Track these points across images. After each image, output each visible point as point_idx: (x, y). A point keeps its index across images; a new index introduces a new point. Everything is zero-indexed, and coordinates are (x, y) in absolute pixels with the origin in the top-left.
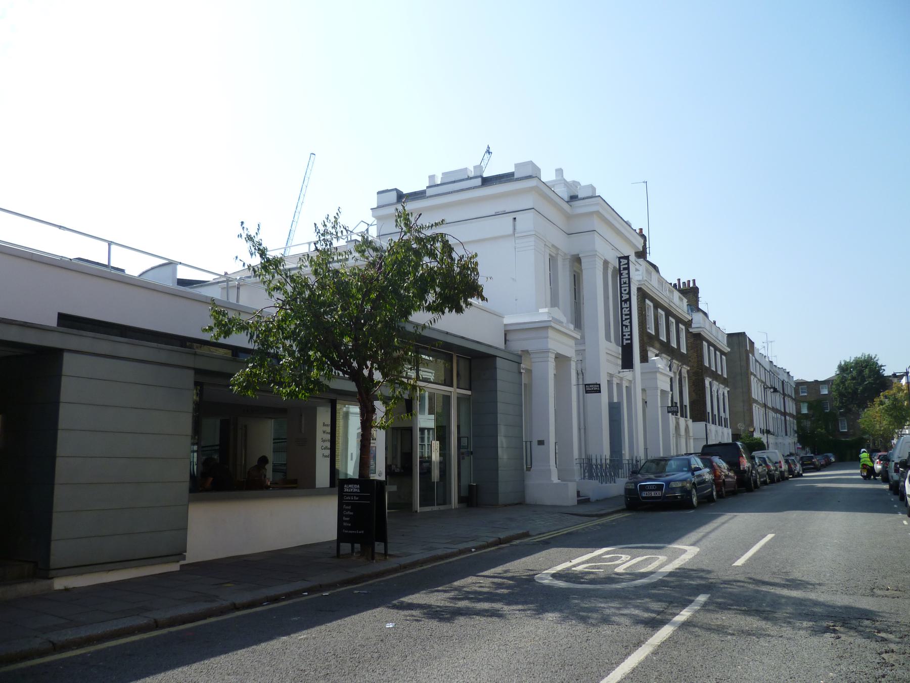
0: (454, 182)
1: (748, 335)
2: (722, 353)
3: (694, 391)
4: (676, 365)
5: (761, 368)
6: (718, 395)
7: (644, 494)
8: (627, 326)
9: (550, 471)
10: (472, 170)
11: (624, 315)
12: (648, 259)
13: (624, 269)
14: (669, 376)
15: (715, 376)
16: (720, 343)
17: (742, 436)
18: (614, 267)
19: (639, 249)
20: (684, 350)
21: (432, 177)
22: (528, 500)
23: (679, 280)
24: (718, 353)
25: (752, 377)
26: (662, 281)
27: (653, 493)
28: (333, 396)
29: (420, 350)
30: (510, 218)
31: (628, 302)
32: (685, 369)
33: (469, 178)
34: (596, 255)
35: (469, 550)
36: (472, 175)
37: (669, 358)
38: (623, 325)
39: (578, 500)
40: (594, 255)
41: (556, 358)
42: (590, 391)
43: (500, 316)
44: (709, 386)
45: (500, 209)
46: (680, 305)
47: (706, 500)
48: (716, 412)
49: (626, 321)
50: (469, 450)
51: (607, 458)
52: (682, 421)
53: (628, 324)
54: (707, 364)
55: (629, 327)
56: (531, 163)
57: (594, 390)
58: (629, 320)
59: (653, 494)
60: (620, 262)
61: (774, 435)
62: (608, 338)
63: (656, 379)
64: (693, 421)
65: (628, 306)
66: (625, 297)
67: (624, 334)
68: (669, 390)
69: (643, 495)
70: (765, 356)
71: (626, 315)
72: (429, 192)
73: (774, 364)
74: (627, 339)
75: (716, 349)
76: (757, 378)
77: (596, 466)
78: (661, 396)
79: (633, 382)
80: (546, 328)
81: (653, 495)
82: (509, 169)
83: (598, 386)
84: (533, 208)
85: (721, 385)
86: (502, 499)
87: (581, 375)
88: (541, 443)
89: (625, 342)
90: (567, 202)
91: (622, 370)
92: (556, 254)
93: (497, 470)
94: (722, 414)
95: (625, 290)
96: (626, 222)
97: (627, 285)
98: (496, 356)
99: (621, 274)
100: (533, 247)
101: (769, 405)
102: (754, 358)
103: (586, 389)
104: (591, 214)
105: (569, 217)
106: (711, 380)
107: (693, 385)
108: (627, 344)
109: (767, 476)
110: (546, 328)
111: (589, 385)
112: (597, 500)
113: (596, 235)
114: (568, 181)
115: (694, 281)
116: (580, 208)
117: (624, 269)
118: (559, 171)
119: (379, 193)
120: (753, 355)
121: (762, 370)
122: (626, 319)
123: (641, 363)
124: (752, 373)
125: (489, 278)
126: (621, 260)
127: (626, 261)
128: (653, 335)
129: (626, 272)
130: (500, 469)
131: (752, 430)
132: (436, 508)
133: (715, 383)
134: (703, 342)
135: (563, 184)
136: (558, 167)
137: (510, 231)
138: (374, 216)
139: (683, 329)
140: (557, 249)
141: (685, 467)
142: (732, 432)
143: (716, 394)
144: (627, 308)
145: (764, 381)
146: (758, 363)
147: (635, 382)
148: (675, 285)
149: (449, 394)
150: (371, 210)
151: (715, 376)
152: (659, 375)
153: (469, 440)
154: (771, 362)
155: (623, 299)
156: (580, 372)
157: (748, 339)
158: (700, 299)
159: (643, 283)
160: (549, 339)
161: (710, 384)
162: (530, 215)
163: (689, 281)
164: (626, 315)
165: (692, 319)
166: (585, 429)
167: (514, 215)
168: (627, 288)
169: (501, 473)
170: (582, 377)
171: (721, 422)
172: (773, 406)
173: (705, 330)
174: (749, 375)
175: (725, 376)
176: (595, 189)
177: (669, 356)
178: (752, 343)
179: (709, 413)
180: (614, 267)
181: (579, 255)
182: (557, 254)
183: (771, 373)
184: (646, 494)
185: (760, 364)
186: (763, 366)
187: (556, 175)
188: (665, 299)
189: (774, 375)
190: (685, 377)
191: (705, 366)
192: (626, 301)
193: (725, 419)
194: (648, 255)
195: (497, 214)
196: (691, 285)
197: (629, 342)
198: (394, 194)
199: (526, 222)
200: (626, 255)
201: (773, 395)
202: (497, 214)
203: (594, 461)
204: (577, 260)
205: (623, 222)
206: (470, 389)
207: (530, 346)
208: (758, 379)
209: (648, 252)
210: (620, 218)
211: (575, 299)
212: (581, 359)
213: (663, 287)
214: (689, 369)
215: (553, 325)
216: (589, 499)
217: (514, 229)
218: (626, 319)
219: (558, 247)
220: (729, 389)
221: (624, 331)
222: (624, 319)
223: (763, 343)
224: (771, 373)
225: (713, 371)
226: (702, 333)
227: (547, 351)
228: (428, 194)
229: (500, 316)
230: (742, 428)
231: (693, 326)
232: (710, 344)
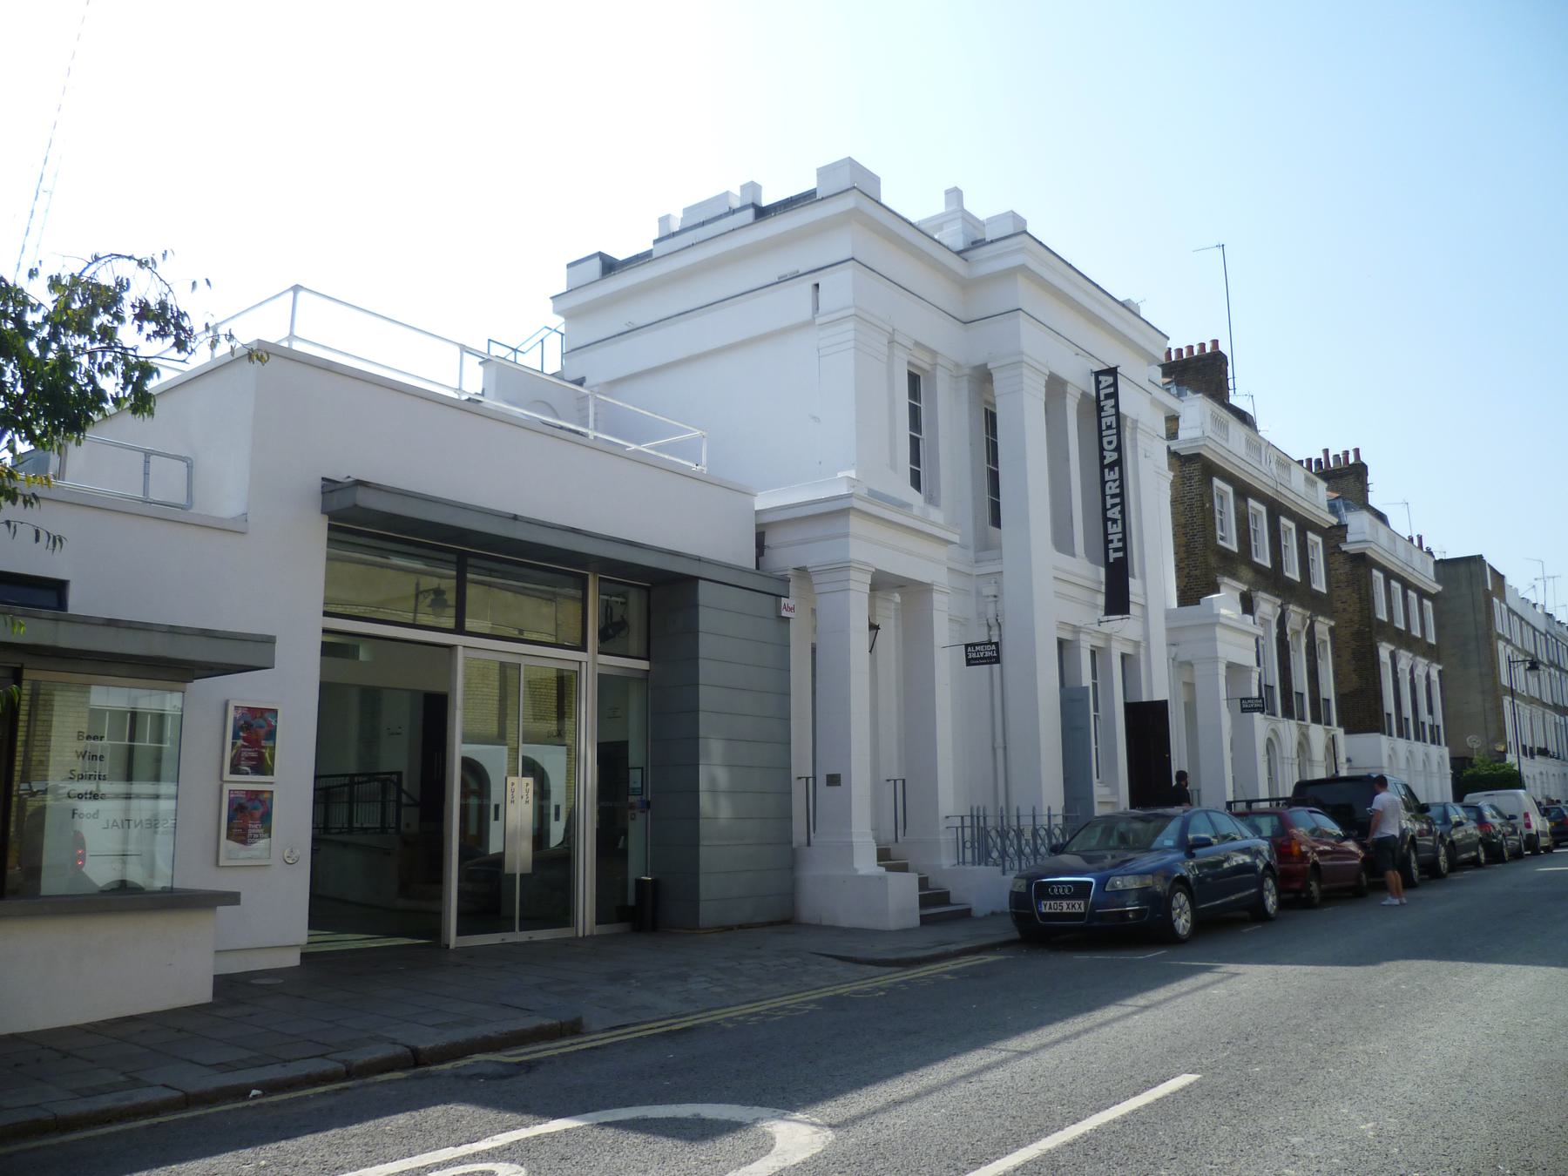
0: (703, 224)
1: (1488, 561)
2: (1422, 594)
3: (1355, 670)
4: (1300, 618)
5: (1525, 627)
6: (1412, 679)
7: (1047, 907)
8: (1115, 521)
9: (852, 846)
10: (738, 193)
11: (1108, 498)
12: (1233, 400)
13: (1108, 396)
14: (1253, 634)
15: (1404, 640)
16: (1415, 574)
17: (1474, 761)
18: (1084, 395)
19: (1159, 360)
20: (1320, 585)
21: (664, 221)
22: (807, 913)
23: (1326, 451)
24: (1395, 585)
25: (1501, 645)
26: (1258, 445)
27: (1065, 904)
28: (14, 660)
29: (471, 561)
30: (806, 285)
31: (1117, 469)
32: (1323, 626)
33: (733, 212)
34: (1022, 362)
35: (241, 1093)
36: (736, 204)
37: (1279, 602)
38: (1106, 519)
39: (921, 916)
41: (874, 588)
42: (976, 659)
43: (745, 493)
44: (1389, 662)
45: (788, 269)
46: (1316, 500)
47: (1246, 914)
48: (1407, 711)
49: (1113, 510)
50: (644, 798)
51: (987, 813)
52: (1317, 734)
53: (1118, 516)
54: (1382, 615)
55: (1119, 522)
56: (851, 163)
57: (986, 658)
58: (1119, 508)
59: (1065, 906)
60: (1098, 383)
61: (1558, 758)
62: (1062, 542)
63: (1214, 639)
64: (1347, 732)
65: (1117, 476)
66: (1111, 457)
67: (1110, 537)
68: (1255, 664)
69: (1044, 911)
70: (1535, 605)
71: (1113, 496)
73: (1557, 619)
74: (1116, 550)
75: (1406, 585)
76: (1513, 645)
78: (1227, 678)
79: (1143, 644)
80: (844, 513)
82: (807, 183)
83: (994, 647)
84: (853, 259)
85: (1419, 659)
86: (708, 912)
87: (997, 628)
88: (833, 780)
89: (1113, 556)
91: (1106, 618)
92: (931, 365)
93: (696, 845)
94: (1424, 716)
95: (1110, 443)
96: (1123, 304)
97: (1115, 431)
98: (697, 578)
99: (1100, 409)
100: (852, 344)
101: (1545, 701)
102: (1504, 606)
103: (967, 656)
104: (1011, 273)
105: (966, 286)
106: (1392, 648)
108: (1115, 559)
109: (1481, 848)
110: (844, 513)
111: (974, 645)
112: (993, 914)
113: (1024, 323)
114: (981, 219)
115: (1357, 451)
116: (987, 263)
117: (1108, 396)
118: (955, 195)
119: (569, 266)
120: (1503, 599)
121: (1528, 633)
122: (1113, 506)
124: (1500, 637)
125: (201, 284)
126: (1101, 378)
127: (1110, 380)
128: (1233, 552)
129: (1111, 402)
130: (703, 842)
131: (1502, 748)
132: (519, 936)
133: (1405, 659)
134: (1371, 571)
135: (960, 220)
136: (950, 186)
137: (805, 312)
138: (558, 312)
139: (1317, 544)
140: (933, 353)
141: (1439, 819)
142: (1450, 753)
143: (1408, 677)
144: (1114, 481)
145: (1533, 652)
146: (1515, 618)
147: (1148, 643)
148: (1319, 462)
149: (575, 667)
150: (551, 301)
151: (1404, 640)
152: (1219, 632)
153: (645, 773)
154: (1550, 616)
155: (1106, 462)
156: (992, 621)
157: (1488, 570)
158: (1371, 488)
159: (1202, 443)
160: (851, 539)
161: (1394, 657)
162: (846, 274)
163: (1346, 453)
164: (1113, 496)
166: (1005, 748)
167: (814, 279)
168: (1114, 438)
169: (709, 856)
170: (997, 632)
172: (1556, 701)
173: (1374, 547)
174: (1494, 639)
175: (1432, 640)
176: (962, 192)
177: (1278, 596)
178: (1499, 578)
179: (1389, 715)
180: (1084, 395)
181: (986, 365)
182: (934, 365)
183: (1548, 636)
184: (1050, 908)
185: (1521, 619)
186: (1528, 623)
187: (947, 203)
188: (1264, 479)
189: (1557, 640)
190: (1325, 642)
191: (1396, 628)
192: (1111, 466)
193: (1432, 727)
194: (1231, 392)
195: (783, 280)
196: (1352, 460)
197: (1120, 554)
198: (597, 262)
199: (839, 288)
200: (1112, 366)
201: (1530, 678)
202: (783, 280)
203: (991, 822)
204: (983, 377)
205: (1115, 304)
206: (647, 659)
207: (812, 557)
208: (1518, 649)
209: (1231, 386)
210: (1094, 288)
212: (993, 593)
213: (1261, 457)
214: (1332, 623)
215: (857, 504)
216: (969, 910)
217: (816, 308)
218: (1113, 506)
219: (935, 349)
220: (1440, 667)
221: (1110, 531)
222: (1108, 506)
223: (1536, 579)
224: (1548, 636)
225: (1399, 630)
226: (1369, 553)
227: (844, 567)
228: (655, 255)
229: (745, 493)
230: (1476, 746)
231: (1350, 538)
232: (1389, 575)
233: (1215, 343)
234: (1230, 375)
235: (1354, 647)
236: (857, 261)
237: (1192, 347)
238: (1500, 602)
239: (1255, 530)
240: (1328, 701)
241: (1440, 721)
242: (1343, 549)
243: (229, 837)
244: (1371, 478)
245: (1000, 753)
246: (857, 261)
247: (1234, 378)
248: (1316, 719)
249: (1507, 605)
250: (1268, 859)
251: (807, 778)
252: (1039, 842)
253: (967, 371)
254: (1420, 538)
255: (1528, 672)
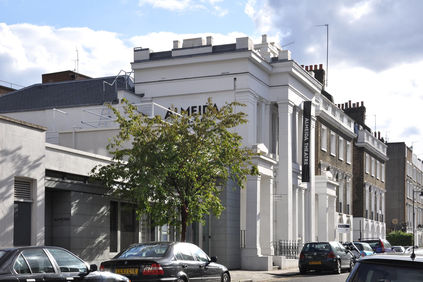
1: (407, 145)
3: (356, 193)
21: (176, 43)
23: (350, 102)
30: (232, 78)
40: (287, 102)
45: (225, 71)
48: (373, 210)
72: (174, 54)
77: (290, 247)
81: (316, 262)
90: (270, 63)
91: (302, 183)
107: (356, 188)
115: (362, 103)
116: (279, 67)
123: (315, 175)
150: (130, 64)
158: (366, 117)
165: (357, 137)
167: (235, 76)
171: (375, 217)
181: (277, 102)
203: (283, 245)
211: (272, 132)
217: (235, 86)
233: (321, 66)
234: (326, 79)
235: (356, 184)
236: (250, 73)
237: (340, 105)
238: (410, 162)
239: (331, 142)
240: (341, 203)
241: (383, 213)
242: (356, 145)
243: (30, 245)
244: (367, 113)
245: (341, 226)
246: (250, 73)
247: (327, 80)
248: (381, 221)
249: (412, 163)
250: (385, 248)
251: (244, 231)
252: (291, 250)
253: (270, 103)
254: (379, 133)
255: (420, 196)
